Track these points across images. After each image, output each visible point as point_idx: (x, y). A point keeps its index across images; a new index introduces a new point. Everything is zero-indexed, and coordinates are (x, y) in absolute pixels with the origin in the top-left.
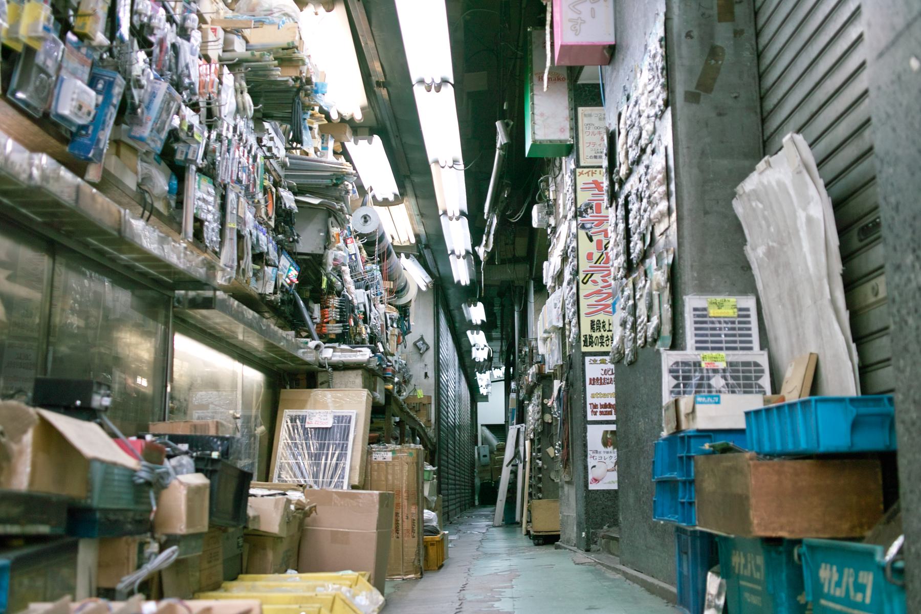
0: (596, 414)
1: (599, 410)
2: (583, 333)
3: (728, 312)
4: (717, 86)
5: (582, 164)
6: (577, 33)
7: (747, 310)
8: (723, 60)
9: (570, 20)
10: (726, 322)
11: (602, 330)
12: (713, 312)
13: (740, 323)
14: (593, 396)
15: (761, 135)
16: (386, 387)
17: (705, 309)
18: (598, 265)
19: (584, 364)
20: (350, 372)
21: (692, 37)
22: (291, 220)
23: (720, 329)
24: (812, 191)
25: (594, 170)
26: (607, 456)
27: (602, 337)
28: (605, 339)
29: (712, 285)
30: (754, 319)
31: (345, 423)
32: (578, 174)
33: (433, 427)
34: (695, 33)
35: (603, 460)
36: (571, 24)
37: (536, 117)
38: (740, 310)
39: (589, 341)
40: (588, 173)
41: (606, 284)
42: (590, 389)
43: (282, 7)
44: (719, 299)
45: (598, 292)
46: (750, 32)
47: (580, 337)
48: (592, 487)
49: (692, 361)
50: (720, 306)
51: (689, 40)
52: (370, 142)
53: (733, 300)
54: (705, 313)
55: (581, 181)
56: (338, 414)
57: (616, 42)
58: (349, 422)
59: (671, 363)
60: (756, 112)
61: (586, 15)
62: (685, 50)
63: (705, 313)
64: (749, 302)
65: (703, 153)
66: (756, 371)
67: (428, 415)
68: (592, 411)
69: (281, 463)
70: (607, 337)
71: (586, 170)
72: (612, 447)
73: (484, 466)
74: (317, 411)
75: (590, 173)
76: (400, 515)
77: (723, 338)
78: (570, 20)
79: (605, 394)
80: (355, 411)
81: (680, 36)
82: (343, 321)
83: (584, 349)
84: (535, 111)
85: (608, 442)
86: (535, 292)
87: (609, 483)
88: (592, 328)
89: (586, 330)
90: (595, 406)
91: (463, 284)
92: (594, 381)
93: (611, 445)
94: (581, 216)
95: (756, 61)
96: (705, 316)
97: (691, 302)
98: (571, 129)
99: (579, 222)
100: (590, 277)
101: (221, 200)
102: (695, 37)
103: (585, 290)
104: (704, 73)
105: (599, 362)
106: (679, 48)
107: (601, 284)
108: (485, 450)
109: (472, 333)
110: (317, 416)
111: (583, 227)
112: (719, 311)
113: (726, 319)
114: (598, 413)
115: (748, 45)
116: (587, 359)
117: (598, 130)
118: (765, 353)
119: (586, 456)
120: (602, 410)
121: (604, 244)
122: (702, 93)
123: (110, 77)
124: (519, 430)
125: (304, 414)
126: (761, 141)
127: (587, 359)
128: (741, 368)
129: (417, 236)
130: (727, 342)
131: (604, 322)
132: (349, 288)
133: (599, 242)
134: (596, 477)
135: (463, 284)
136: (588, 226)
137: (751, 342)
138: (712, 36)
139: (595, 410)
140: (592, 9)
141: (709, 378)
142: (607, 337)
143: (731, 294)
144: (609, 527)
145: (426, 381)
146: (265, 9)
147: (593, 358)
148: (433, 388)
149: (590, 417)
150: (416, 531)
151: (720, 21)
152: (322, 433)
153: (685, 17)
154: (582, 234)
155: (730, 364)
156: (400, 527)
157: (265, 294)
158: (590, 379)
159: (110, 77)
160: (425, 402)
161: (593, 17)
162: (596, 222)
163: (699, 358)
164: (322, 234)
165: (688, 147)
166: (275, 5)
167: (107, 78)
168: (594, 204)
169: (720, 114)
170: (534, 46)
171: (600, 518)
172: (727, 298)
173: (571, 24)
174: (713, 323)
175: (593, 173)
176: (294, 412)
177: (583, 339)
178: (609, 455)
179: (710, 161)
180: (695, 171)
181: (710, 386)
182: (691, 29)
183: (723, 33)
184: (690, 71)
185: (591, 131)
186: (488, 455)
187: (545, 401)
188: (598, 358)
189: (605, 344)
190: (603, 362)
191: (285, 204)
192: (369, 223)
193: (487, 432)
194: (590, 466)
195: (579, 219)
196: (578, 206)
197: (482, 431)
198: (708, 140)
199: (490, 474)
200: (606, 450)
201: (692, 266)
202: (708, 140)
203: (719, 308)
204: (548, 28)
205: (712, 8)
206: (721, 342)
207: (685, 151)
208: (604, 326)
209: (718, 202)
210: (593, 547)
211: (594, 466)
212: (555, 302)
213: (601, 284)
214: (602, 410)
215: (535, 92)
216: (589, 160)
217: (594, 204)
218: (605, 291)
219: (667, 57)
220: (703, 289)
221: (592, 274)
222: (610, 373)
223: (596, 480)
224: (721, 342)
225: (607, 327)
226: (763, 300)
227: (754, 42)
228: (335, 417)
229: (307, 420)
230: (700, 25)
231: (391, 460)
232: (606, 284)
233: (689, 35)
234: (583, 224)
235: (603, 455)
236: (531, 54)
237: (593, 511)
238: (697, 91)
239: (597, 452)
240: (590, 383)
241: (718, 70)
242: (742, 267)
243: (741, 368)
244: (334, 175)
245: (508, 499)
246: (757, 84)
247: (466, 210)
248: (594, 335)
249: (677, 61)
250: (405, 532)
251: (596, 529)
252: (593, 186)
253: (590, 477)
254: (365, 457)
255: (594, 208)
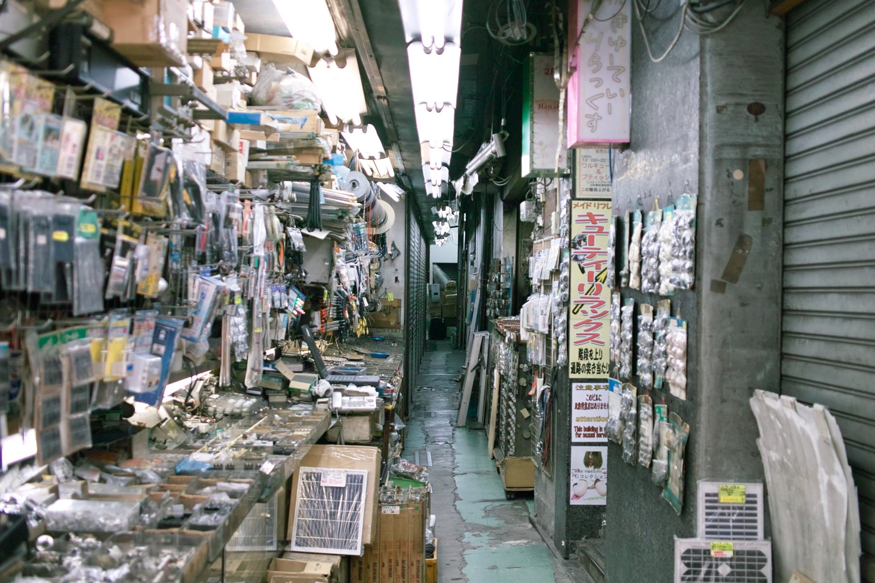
0: (579, 437)
1: (582, 432)
2: (571, 361)
3: (737, 498)
4: (742, 275)
5: (578, 196)
6: (593, 129)
7: (755, 496)
8: (749, 250)
9: (587, 116)
10: (734, 508)
11: (589, 358)
12: (724, 498)
13: (747, 508)
14: (578, 420)
15: (780, 326)
16: (386, 407)
17: (716, 495)
18: (588, 296)
19: (571, 390)
20: (358, 418)
21: (722, 226)
22: (299, 258)
23: (729, 514)
24: (837, 467)
25: (589, 202)
26: (588, 474)
27: (589, 364)
28: (592, 367)
29: (724, 469)
30: (760, 506)
31: (358, 482)
32: (573, 206)
33: (402, 329)
34: (725, 222)
35: (584, 478)
36: (587, 120)
37: (535, 146)
38: (748, 496)
39: (577, 369)
40: (583, 205)
41: (595, 314)
42: (576, 413)
43: (301, 93)
44: (729, 485)
45: (587, 322)
46: (777, 221)
47: (568, 364)
48: (573, 502)
49: (703, 548)
50: (730, 492)
51: (719, 228)
52: (365, 131)
53: (742, 487)
54: (716, 498)
55: (576, 212)
56: (350, 473)
57: (630, 139)
58: (362, 482)
59: (683, 550)
60: (777, 303)
61: (603, 111)
62: (714, 238)
63: (716, 498)
64: (756, 489)
65: (725, 343)
66: (760, 560)
67: (398, 317)
68: (576, 434)
69: (299, 520)
70: (594, 365)
71: (581, 202)
72: (593, 467)
73: (434, 303)
74: (332, 469)
75: (585, 205)
76: (406, 562)
77: (731, 524)
78: (587, 116)
79: (588, 418)
80: (366, 471)
81: (710, 223)
82: (339, 317)
83: (571, 376)
84: (535, 140)
85: (589, 462)
86: (505, 213)
87: (589, 499)
88: (580, 356)
89: (574, 357)
90: (579, 429)
91: (435, 196)
92: (579, 406)
93: (593, 464)
94: (575, 247)
95: (781, 251)
96: (716, 501)
97: (704, 488)
98: (569, 158)
99: (572, 253)
100: (581, 307)
101: (249, 308)
102: (725, 225)
103: (574, 319)
104: (731, 263)
105: (585, 388)
106: (709, 235)
107: (591, 314)
108: (436, 288)
109: (438, 224)
110: (331, 474)
111: (576, 259)
112: (730, 497)
113: (735, 505)
114: (582, 436)
115: (774, 235)
116: (574, 385)
117: (594, 163)
118: (768, 544)
119: (569, 474)
120: (586, 432)
121: (595, 276)
122: (728, 283)
123: (172, 327)
124: (483, 338)
125: (320, 471)
126: (779, 331)
127: (574, 385)
128: (746, 557)
129: (396, 170)
130: (734, 527)
131: (591, 351)
132: (345, 283)
133: (591, 274)
134: (577, 493)
135: (435, 196)
136: (581, 258)
137: (755, 521)
138: (741, 225)
139: (579, 433)
140: (609, 104)
141: (717, 566)
142: (594, 365)
143: (740, 479)
144: (586, 538)
145: (396, 285)
146: (284, 95)
147: (579, 384)
148: (403, 291)
149: (574, 439)
150: (421, 576)
151: (750, 209)
152: (336, 492)
153: (717, 204)
154: (575, 265)
155: (737, 553)
156: (406, 573)
157: (278, 341)
158: (576, 404)
159: (172, 327)
160: (396, 305)
161: (610, 113)
162: (589, 254)
163: (709, 547)
164: (327, 264)
165: (711, 336)
166: (294, 91)
167: (169, 328)
168: (587, 236)
169: (743, 305)
170: (536, 72)
171: (578, 530)
172: (737, 485)
173: (587, 120)
174: (723, 508)
175: (587, 205)
176: (308, 469)
177: (571, 366)
178: (590, 474)
179: (730, 350)
180: (716, 360)
181: (717, 573)
182: (721, 217)
183: (752, 221)
184: (718, 260)
185: (587, 163)
186: (439, 292)
187: (521, 366)
188: (584, 385)
189: (591, 372)
190: (589, 388)
191: (294, 245)
192: (357, 187)
193: (439, 271)
194: (572, 484)
195: (573, 250)
196: (573, 238)
197: (434, 268)
198: (730, 329)
199: (440, 311)
200: (587, 469)
201: (706, 451)
202: (730, 329)
203: (729, 495)
204: (561, 112)
205: (743, 195)
206: (728, 527)
207: (708, 339)
208: (591, 355)
209: (735, 391)
210: (571, 555)
211: (576, 484)
212: (542, 309)
213: (591, 314)
214: (586, 432)
215: (535, 121)
216: (585, 193)
217: (587, 236)
218: (593, 321)
219: (697, 241)
220: (715, 476)
221: (582, 305)
222: (595, 398)
223: (577, 497)
224: (728, 527)
225: (594, 356)
226: (768, 487)
227: (780, 232)
228: (348, 476)
229: (322, 478)
230: (730, 213)
231: (398, 513)
232: (595, 314)
233: (719, 223)
234: (576, 256)
235: (584, 474)
236: (533, 81)
237: (573, 524)
238: (724, 281)
239: (579, 471)
240: (576, 408)
241: (744, 259)
242: (752, 454)
243: (746, 557)
244: (340, 209)
245: (472, 395)
246: (780, 274)
247: (449, 163)
248: (582, 362)
249: (705, 248)
250: (410, 577)
251: (575, 539)
252: (588, 218)
253: (572, 494)
254: (376, 511)
255: (587, 241)
